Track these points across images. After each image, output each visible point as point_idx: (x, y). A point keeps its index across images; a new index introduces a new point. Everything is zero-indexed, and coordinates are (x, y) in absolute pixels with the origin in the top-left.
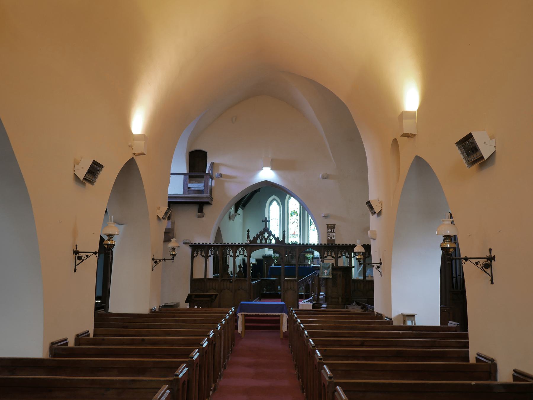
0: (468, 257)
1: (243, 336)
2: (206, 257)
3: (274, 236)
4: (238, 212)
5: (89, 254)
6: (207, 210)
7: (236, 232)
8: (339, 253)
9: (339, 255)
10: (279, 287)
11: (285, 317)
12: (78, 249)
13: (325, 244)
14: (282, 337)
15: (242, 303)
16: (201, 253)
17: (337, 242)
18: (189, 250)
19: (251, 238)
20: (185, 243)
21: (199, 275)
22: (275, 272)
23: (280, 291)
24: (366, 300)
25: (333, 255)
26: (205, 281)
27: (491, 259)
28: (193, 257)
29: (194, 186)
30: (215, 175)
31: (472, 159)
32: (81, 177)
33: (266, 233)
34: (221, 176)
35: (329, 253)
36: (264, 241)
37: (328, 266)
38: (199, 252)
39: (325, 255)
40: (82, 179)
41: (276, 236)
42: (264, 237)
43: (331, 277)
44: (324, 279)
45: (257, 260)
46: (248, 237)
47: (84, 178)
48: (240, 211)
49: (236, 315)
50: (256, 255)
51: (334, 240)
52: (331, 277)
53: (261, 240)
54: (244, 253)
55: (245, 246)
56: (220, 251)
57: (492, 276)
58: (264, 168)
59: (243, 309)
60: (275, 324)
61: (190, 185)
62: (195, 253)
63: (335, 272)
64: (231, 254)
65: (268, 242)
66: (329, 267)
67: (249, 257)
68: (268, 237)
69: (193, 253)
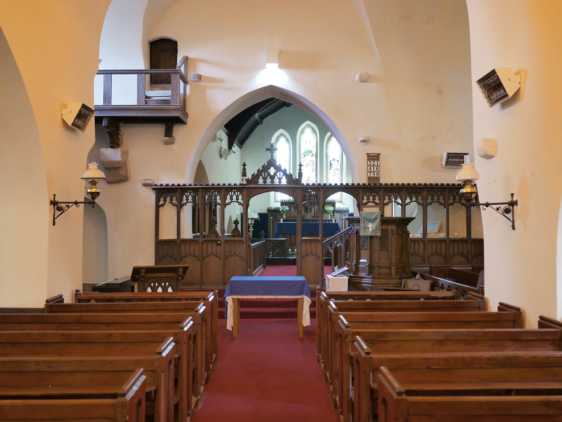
0: (489, 202)
1: (235, 335)
2: (180, 207)
3: (284, 172)
4: (233, 149)
5: (70, 205)
6: (178, 131)
7: (228, 170)
8: (387, 198)
9: (386, 202)
10: (290, 250)
11: (307, 302)
12: (56, 199)
13: (364, 184)
14: (301, 335)
15: (234, 278)
16: (171, 200)
17: (383, 181)
18: (151, 196)
19: (249, 176)
20: (145, 185)
21: (168, 233)
22: (288, 229)
23: (291, 255)
24: (428, 269)
25: (443, 202)
26: (178, 243)
27: (513, 204)
28: (158, 207)
29: (158, 94)
30: (190, 77)
31: (495, 95)
32: (70, 122)
33: (272, 168)
34: (200, 77)
35: (371, 198)
36: (269, 181)
37: (374, 217)
38: (168, 199)
39: (365, 201)
40: (70, 124)
41: (288, 173)
42: (269, 174)
43: (379, 234)
44: (366, 237)
45: (260, 215)
46: (244, 174)
47: (73, 124)
48: (235, 148)
49: (223, 304)
50: (258, 205)
51: (378, 178)
52: (379, 234)
53: (265, 179)
54: (237, 199)
55: (240, 189)
56: (204, 196)
57: (513, 222)
58: (268, 65)
59: (236, 289)
60: (290, 311)
61: (150, 93)
62: (162, 199)
63: (384, 227)
64: (219, 201)
65: (276, 181)
66: (376, 219)
67: (246, 206)
68: (275, 174)
69: (158, 201)
